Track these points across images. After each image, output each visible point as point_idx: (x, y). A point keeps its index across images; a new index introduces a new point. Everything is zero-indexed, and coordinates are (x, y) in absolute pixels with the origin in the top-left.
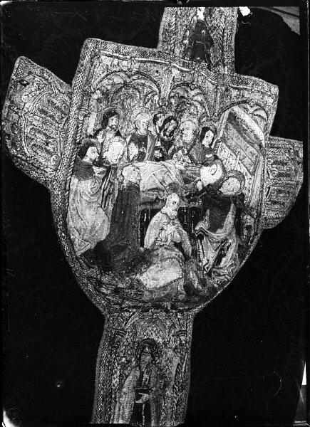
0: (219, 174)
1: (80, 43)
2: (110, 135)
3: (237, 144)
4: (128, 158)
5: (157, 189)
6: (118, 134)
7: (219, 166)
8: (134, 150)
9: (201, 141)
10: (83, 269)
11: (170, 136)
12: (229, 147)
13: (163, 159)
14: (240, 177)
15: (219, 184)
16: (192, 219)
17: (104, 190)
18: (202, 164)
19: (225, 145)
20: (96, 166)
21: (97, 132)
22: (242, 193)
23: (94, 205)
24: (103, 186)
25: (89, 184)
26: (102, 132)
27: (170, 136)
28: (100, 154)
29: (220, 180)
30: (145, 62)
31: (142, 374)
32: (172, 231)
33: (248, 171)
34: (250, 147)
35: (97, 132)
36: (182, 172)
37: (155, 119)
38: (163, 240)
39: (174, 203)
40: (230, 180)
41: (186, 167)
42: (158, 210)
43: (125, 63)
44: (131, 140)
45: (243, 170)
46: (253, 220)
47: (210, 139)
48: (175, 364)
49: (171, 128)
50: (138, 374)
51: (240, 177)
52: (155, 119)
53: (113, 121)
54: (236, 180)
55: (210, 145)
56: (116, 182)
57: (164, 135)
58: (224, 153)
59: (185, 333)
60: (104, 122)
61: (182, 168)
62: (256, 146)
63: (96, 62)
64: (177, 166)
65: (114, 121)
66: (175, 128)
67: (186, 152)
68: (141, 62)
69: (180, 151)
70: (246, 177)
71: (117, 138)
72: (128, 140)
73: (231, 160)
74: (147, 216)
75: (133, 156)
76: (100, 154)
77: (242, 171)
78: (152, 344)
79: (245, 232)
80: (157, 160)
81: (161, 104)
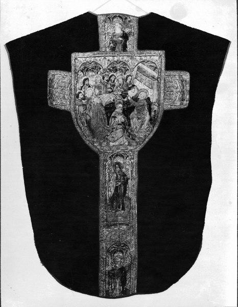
0: (136, 92)
1: (47, 72)
4: (95, 94)
6: (89, 87)
8: (97, 91)
15: (137, 95)
31: (117, 175)
32: (121, 119)
33: (149, 87)
39: (120, 107)
43: (88, 59)
45: (146, 88)
46: (157, 107)
48: (130, 170)
49: (113, 79)
50: (115, 175)
58: (137, 83)
59: (133, 159)
63: (76, 61)
71: (89, 88)
78: (118, 164)
79: (153, 113)
80: (110, 92)
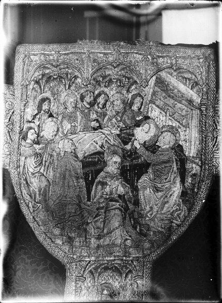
0: (153, 131)
2: (45, 117)
3: (165, 103)
5: (99, 153)
6: (51, 116)
7: (152, 126)
8: (67, 126)
9: (131, 108)
10: (39, 226)
11: (103, 107)
12: (158, 106)
13: (100, 127)
14: (173, 130)
16: (135, 174)
17: (46, 161)
18: (135, 126)
19: (154, 106)
20: (36, 144)
21: (35, 117)
22: (179, 145)
23: (37, 174)
24: (44, 159)
25: (33, 159)
26: (38, 116)
27: (103, 107)
28: (38, 135)
29: (155, 136)
30: (68, 54)
34: (178, 104)
35: (35, 117)
36: (118, 135)
37: (82, 98)
38: (109, 193)
39: (116, 162)
40: (164, 134)
41: (121, 131)
42: (101, 170)
44: (63, 117)
47: (139, 105)
51: (173, 130)
52: (82, 98)
53: (45, 107)
54: (169, 134)
55: (139, 109)
56: (55, 154)
57: (98, 107)
58: (155, 113)
60: (40, 108)
61: (118, 132)
62: (184, 102)
64: (113, 132)
65: (46, 106)
66: (106, 101)
67: (119, 119)
68: (65, 54)
69: (114, 119)
70: (179, 130)
71: (50, 119)
72: (60, 118)
73: (161, 118)
74: (92, 176)
75: (67, 130)
76: (38, 135)
77: (174, 125)
79: (190, 180)
80: (95, 129)
81: (85, 84)
